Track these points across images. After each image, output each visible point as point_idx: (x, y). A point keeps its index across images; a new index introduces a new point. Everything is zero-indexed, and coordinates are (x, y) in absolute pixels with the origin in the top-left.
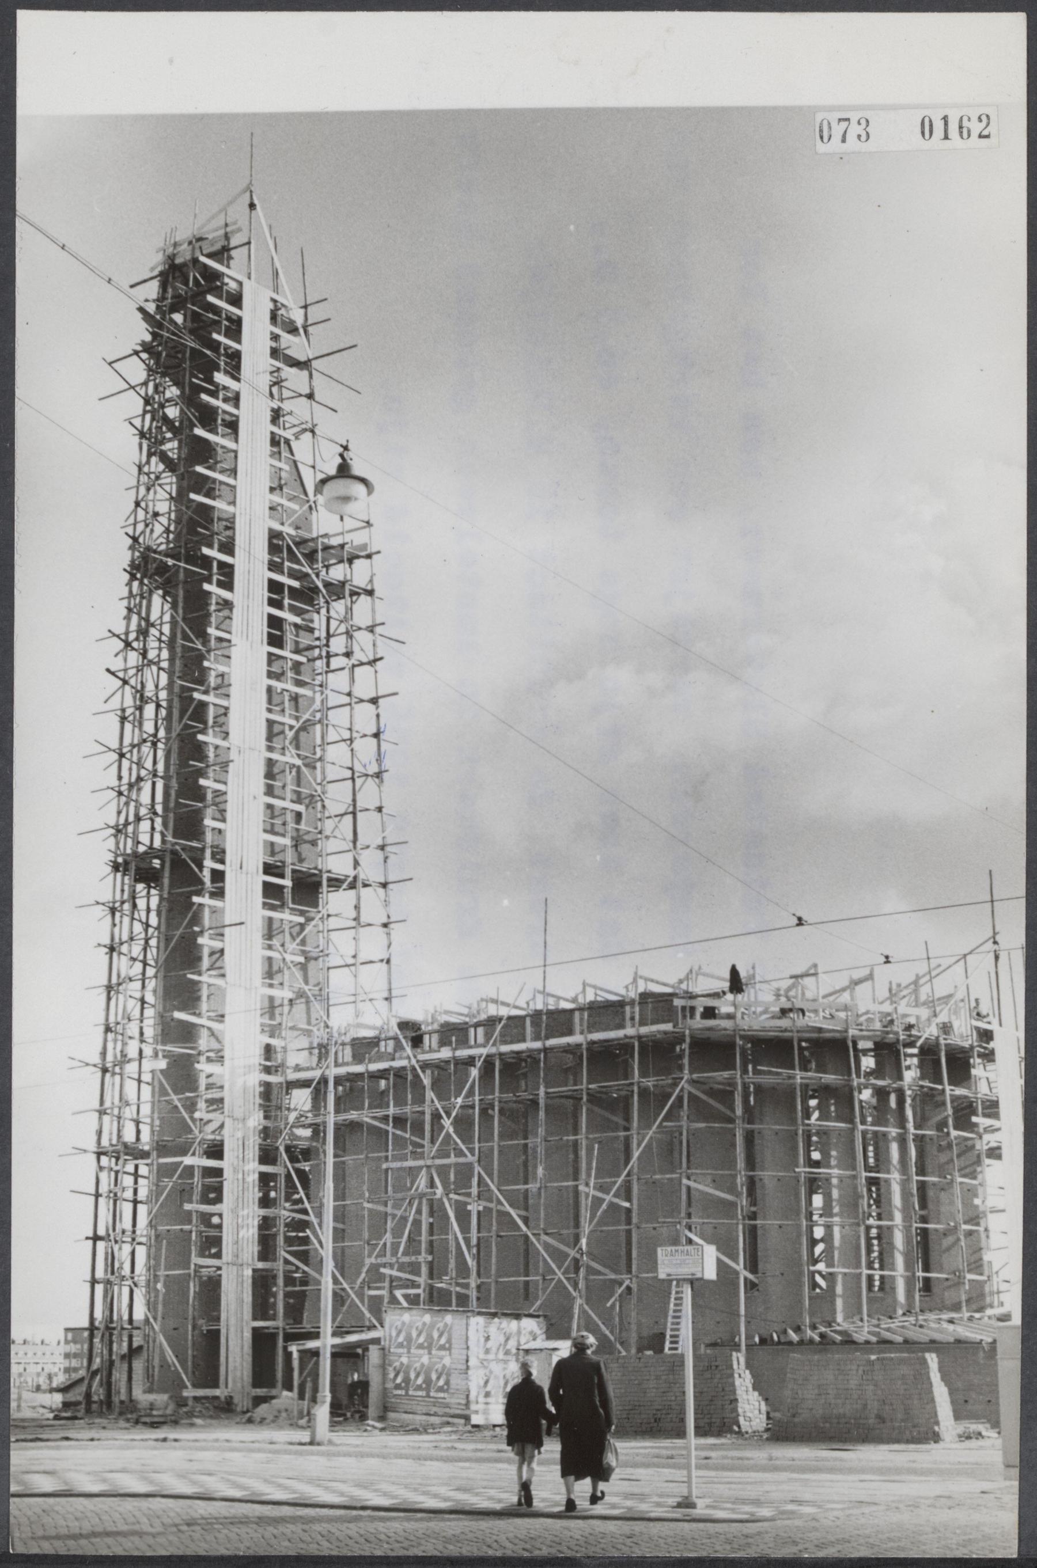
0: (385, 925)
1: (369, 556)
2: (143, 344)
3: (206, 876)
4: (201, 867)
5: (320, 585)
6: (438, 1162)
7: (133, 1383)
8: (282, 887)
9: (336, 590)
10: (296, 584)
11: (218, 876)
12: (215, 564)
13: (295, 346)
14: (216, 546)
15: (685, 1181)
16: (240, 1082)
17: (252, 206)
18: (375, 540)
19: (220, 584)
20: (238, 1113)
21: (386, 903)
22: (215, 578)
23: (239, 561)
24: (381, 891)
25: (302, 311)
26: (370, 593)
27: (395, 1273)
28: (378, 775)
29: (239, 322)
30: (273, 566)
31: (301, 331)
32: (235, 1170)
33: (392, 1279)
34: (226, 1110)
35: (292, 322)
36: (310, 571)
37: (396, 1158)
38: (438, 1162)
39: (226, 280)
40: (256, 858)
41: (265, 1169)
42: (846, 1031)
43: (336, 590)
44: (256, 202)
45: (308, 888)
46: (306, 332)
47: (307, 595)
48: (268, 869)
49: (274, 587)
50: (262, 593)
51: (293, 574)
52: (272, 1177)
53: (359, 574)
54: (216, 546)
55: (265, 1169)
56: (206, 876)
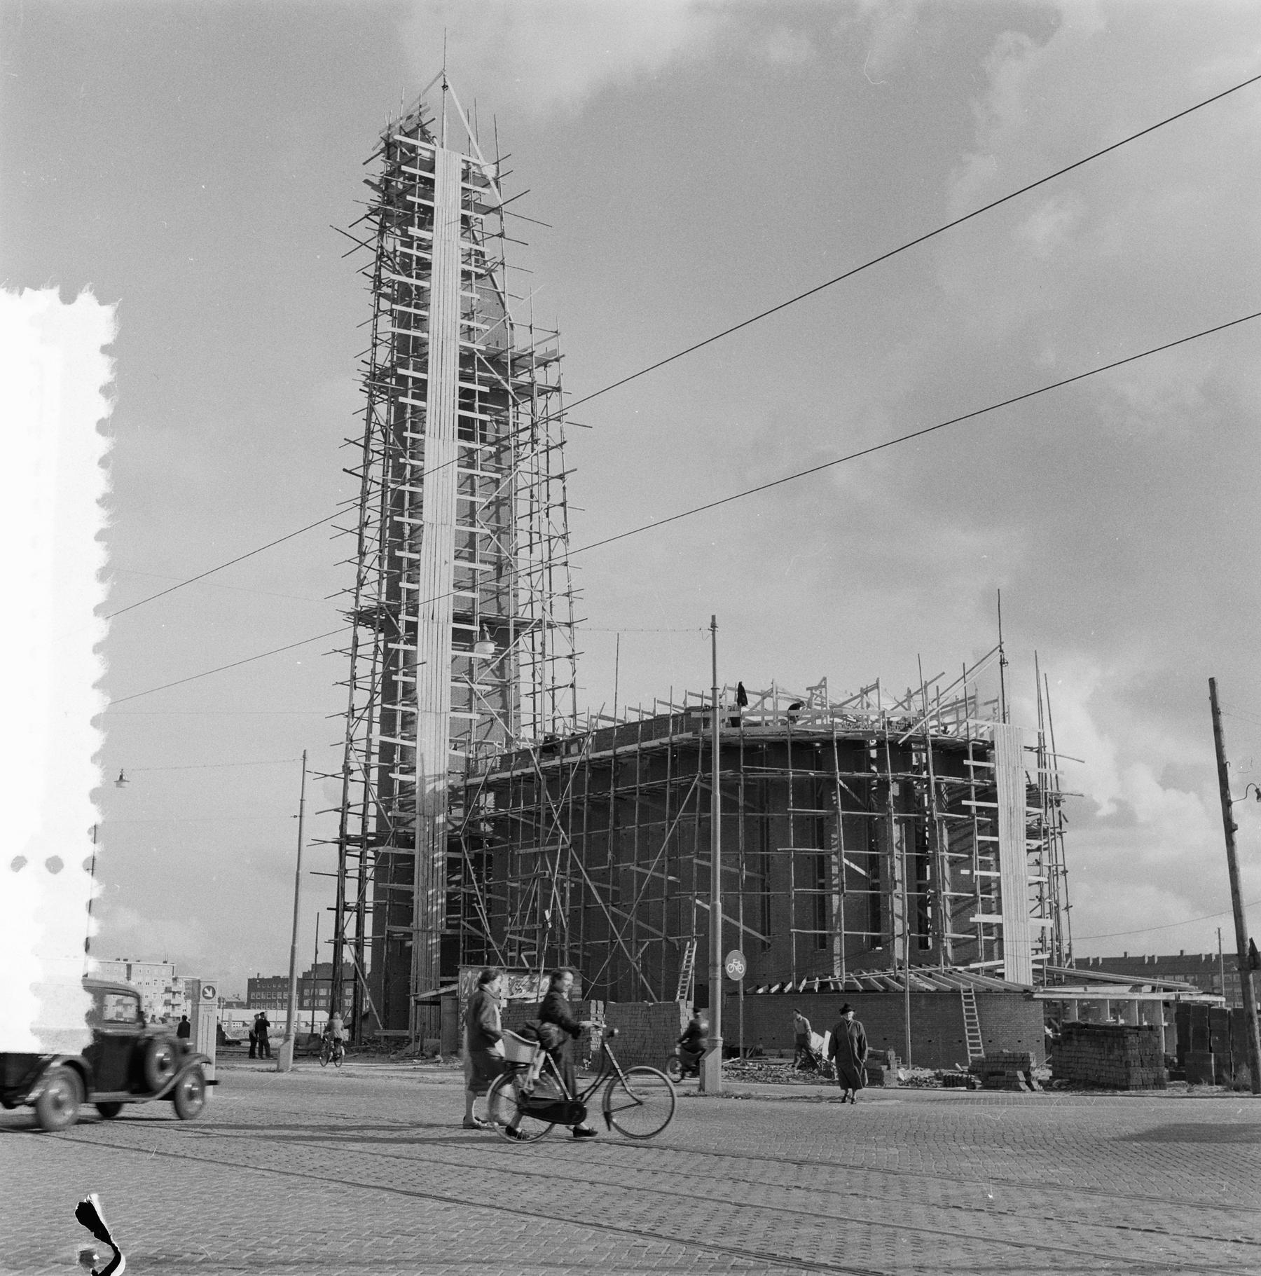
0: (570, 657)
1: (557, 360)
2: (375, 205)
3: (402, 628)
4: (397, 620)
5: (510, 389)
6: (548, 848)
7: (1231, 908)
8: (472, 632)
9: (525, 392)
10: (486, 389)
11: (412, 627)
12: (410, 381)
13: (490, 196)
14: (411, 366)
15: (695, 861)
16: (429, 788)
17: (445, 87)
18: (560, 345)
19: (414, 396)
20: (429, 811)
21: (572, 638)
22: (410, 393)
23: (432, 377)
24: (567, 630)
25: (494, 167)
26: (558, 389)
27: (522, 939)
28: (564, 537)
29: (430, 183)
30: (463, 377)
31: (493, 183)
32: (426, 856)
33: (521, 943)
34: (417, 810)
35: (484, 177)
36: (500, 378)
37: (525, 846)
38: (548, 848)
39: (420, 151)
40: (446, 609)
41: (452, 855)
42: (832, 733)
43: (525, 392)
44: (448, 83)
45: (500, 631)
46: (497, 183)
47: (497, 396)
48: (457, 618)
49: (465, 393)
50: (453, 399)
51: (482, 381)
52: (457, 861)
53: (541, 377)
54: (411, 366)
55: (452, 855)
56: (402, 628)
